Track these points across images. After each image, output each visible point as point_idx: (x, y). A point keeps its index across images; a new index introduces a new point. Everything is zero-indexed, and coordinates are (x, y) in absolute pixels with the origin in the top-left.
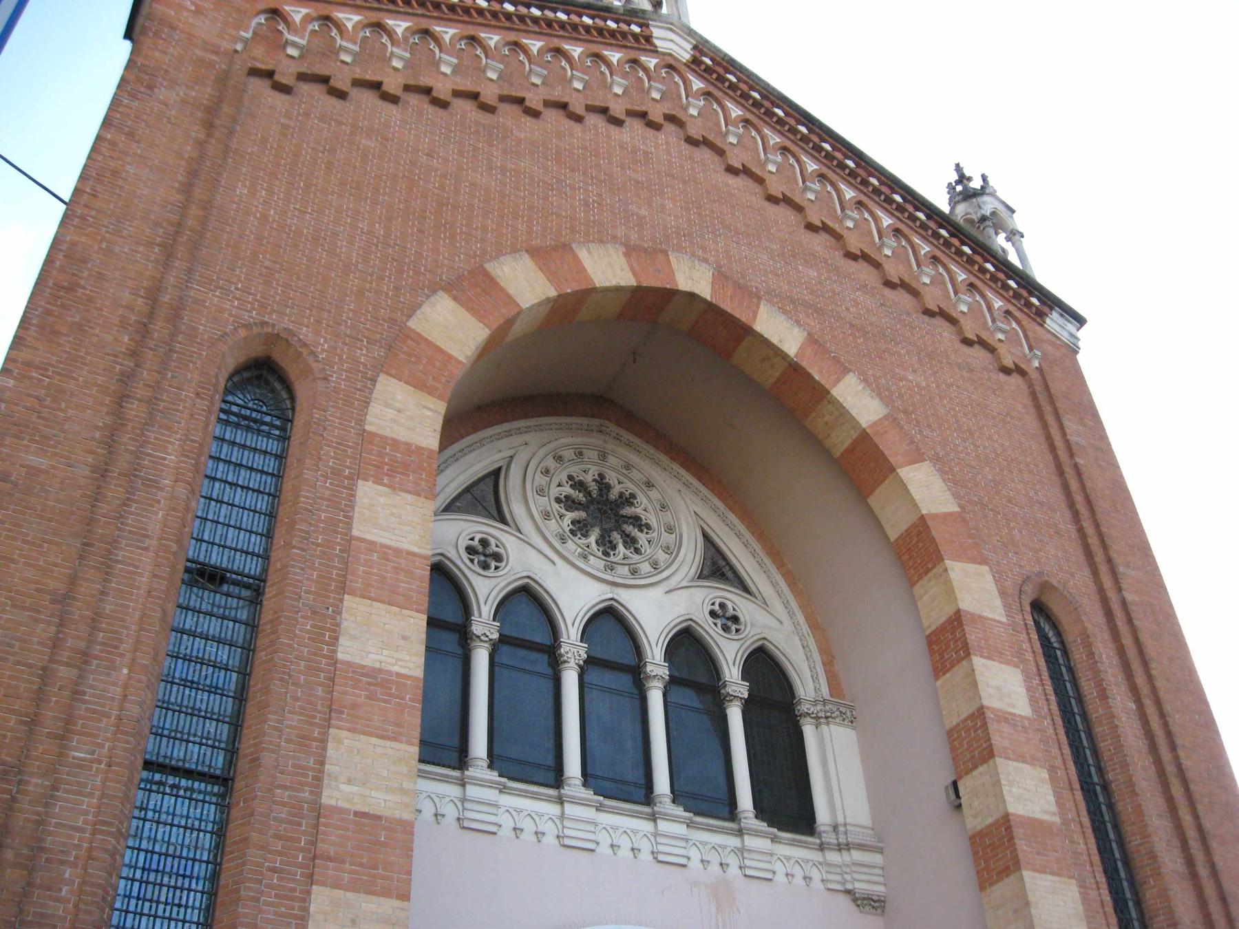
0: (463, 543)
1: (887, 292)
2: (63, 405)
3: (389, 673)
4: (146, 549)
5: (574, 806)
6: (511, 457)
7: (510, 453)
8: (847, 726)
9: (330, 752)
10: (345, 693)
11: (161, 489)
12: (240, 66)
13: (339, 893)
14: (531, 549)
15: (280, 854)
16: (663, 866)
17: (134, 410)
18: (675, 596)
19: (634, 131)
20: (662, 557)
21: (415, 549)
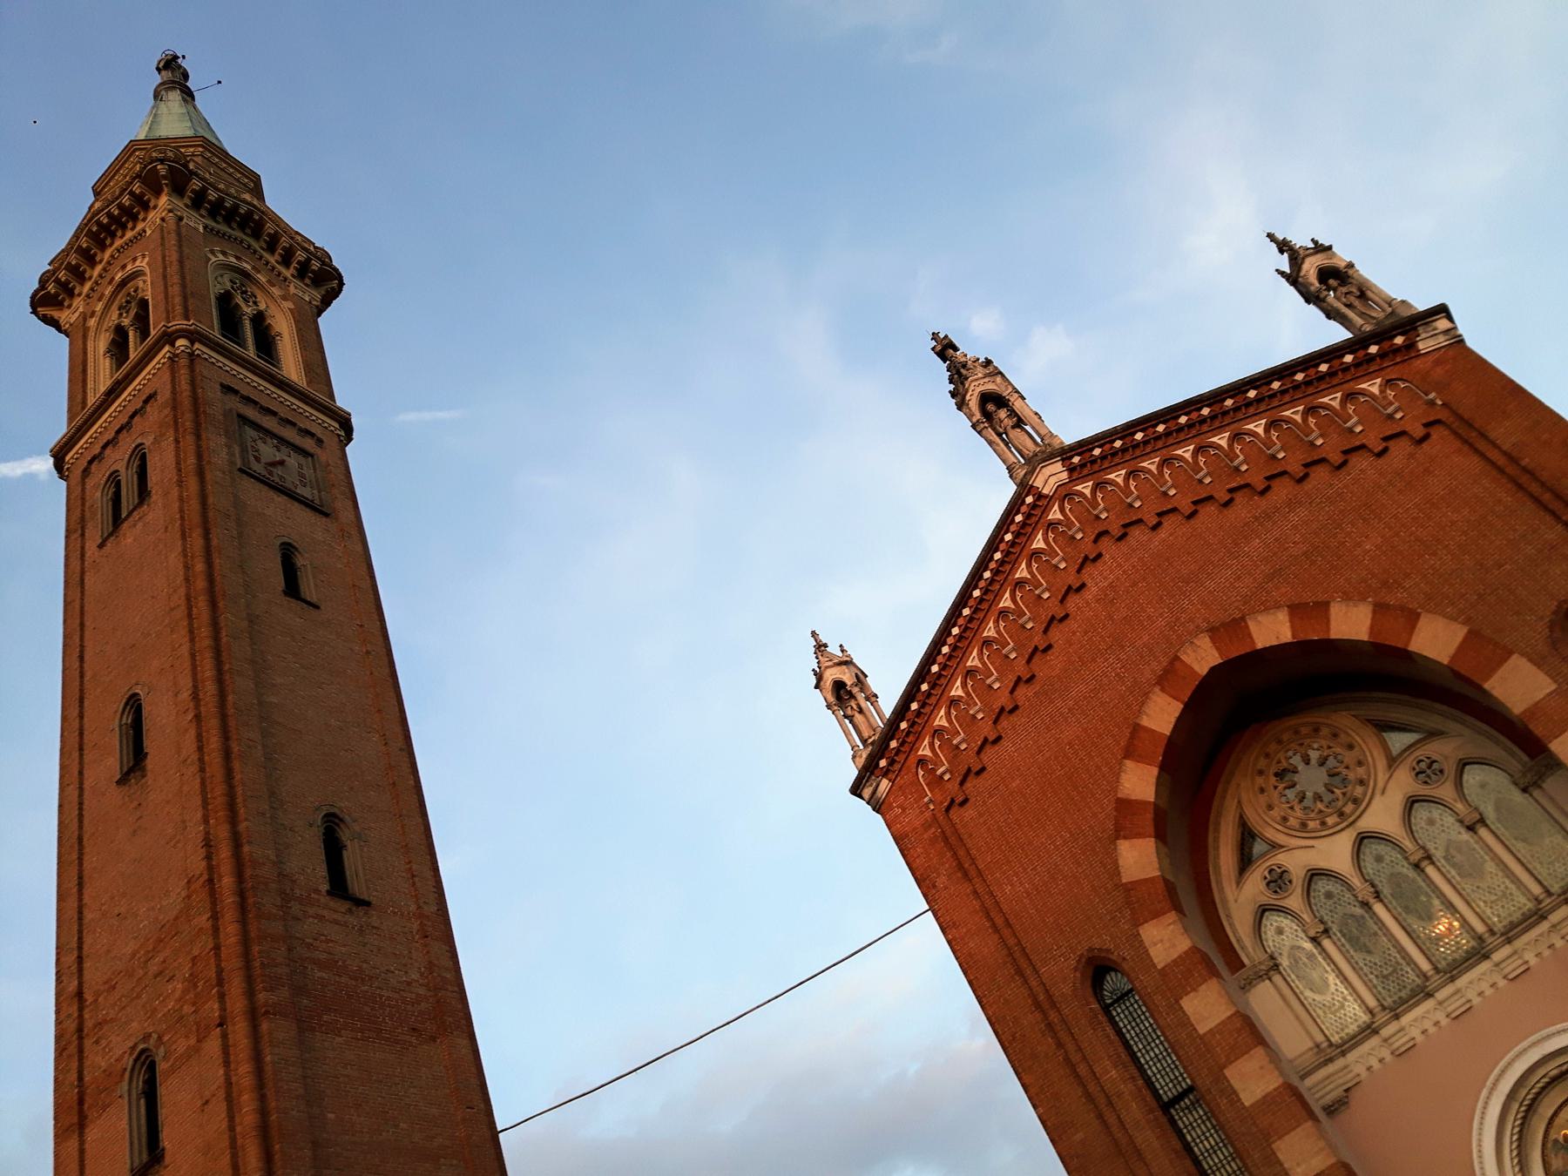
0: (1262, 886)
1: (1308, 485)
2: (1063, 1100)
5: (1440, 992)
6: (1239, 802)
11: (1123, 1093)
14: (1294, 851)
16: (1519, 979)
17: (1082, 1069)
18: (1389, 791)
19: (1096, 579)
20: (1361, 771)
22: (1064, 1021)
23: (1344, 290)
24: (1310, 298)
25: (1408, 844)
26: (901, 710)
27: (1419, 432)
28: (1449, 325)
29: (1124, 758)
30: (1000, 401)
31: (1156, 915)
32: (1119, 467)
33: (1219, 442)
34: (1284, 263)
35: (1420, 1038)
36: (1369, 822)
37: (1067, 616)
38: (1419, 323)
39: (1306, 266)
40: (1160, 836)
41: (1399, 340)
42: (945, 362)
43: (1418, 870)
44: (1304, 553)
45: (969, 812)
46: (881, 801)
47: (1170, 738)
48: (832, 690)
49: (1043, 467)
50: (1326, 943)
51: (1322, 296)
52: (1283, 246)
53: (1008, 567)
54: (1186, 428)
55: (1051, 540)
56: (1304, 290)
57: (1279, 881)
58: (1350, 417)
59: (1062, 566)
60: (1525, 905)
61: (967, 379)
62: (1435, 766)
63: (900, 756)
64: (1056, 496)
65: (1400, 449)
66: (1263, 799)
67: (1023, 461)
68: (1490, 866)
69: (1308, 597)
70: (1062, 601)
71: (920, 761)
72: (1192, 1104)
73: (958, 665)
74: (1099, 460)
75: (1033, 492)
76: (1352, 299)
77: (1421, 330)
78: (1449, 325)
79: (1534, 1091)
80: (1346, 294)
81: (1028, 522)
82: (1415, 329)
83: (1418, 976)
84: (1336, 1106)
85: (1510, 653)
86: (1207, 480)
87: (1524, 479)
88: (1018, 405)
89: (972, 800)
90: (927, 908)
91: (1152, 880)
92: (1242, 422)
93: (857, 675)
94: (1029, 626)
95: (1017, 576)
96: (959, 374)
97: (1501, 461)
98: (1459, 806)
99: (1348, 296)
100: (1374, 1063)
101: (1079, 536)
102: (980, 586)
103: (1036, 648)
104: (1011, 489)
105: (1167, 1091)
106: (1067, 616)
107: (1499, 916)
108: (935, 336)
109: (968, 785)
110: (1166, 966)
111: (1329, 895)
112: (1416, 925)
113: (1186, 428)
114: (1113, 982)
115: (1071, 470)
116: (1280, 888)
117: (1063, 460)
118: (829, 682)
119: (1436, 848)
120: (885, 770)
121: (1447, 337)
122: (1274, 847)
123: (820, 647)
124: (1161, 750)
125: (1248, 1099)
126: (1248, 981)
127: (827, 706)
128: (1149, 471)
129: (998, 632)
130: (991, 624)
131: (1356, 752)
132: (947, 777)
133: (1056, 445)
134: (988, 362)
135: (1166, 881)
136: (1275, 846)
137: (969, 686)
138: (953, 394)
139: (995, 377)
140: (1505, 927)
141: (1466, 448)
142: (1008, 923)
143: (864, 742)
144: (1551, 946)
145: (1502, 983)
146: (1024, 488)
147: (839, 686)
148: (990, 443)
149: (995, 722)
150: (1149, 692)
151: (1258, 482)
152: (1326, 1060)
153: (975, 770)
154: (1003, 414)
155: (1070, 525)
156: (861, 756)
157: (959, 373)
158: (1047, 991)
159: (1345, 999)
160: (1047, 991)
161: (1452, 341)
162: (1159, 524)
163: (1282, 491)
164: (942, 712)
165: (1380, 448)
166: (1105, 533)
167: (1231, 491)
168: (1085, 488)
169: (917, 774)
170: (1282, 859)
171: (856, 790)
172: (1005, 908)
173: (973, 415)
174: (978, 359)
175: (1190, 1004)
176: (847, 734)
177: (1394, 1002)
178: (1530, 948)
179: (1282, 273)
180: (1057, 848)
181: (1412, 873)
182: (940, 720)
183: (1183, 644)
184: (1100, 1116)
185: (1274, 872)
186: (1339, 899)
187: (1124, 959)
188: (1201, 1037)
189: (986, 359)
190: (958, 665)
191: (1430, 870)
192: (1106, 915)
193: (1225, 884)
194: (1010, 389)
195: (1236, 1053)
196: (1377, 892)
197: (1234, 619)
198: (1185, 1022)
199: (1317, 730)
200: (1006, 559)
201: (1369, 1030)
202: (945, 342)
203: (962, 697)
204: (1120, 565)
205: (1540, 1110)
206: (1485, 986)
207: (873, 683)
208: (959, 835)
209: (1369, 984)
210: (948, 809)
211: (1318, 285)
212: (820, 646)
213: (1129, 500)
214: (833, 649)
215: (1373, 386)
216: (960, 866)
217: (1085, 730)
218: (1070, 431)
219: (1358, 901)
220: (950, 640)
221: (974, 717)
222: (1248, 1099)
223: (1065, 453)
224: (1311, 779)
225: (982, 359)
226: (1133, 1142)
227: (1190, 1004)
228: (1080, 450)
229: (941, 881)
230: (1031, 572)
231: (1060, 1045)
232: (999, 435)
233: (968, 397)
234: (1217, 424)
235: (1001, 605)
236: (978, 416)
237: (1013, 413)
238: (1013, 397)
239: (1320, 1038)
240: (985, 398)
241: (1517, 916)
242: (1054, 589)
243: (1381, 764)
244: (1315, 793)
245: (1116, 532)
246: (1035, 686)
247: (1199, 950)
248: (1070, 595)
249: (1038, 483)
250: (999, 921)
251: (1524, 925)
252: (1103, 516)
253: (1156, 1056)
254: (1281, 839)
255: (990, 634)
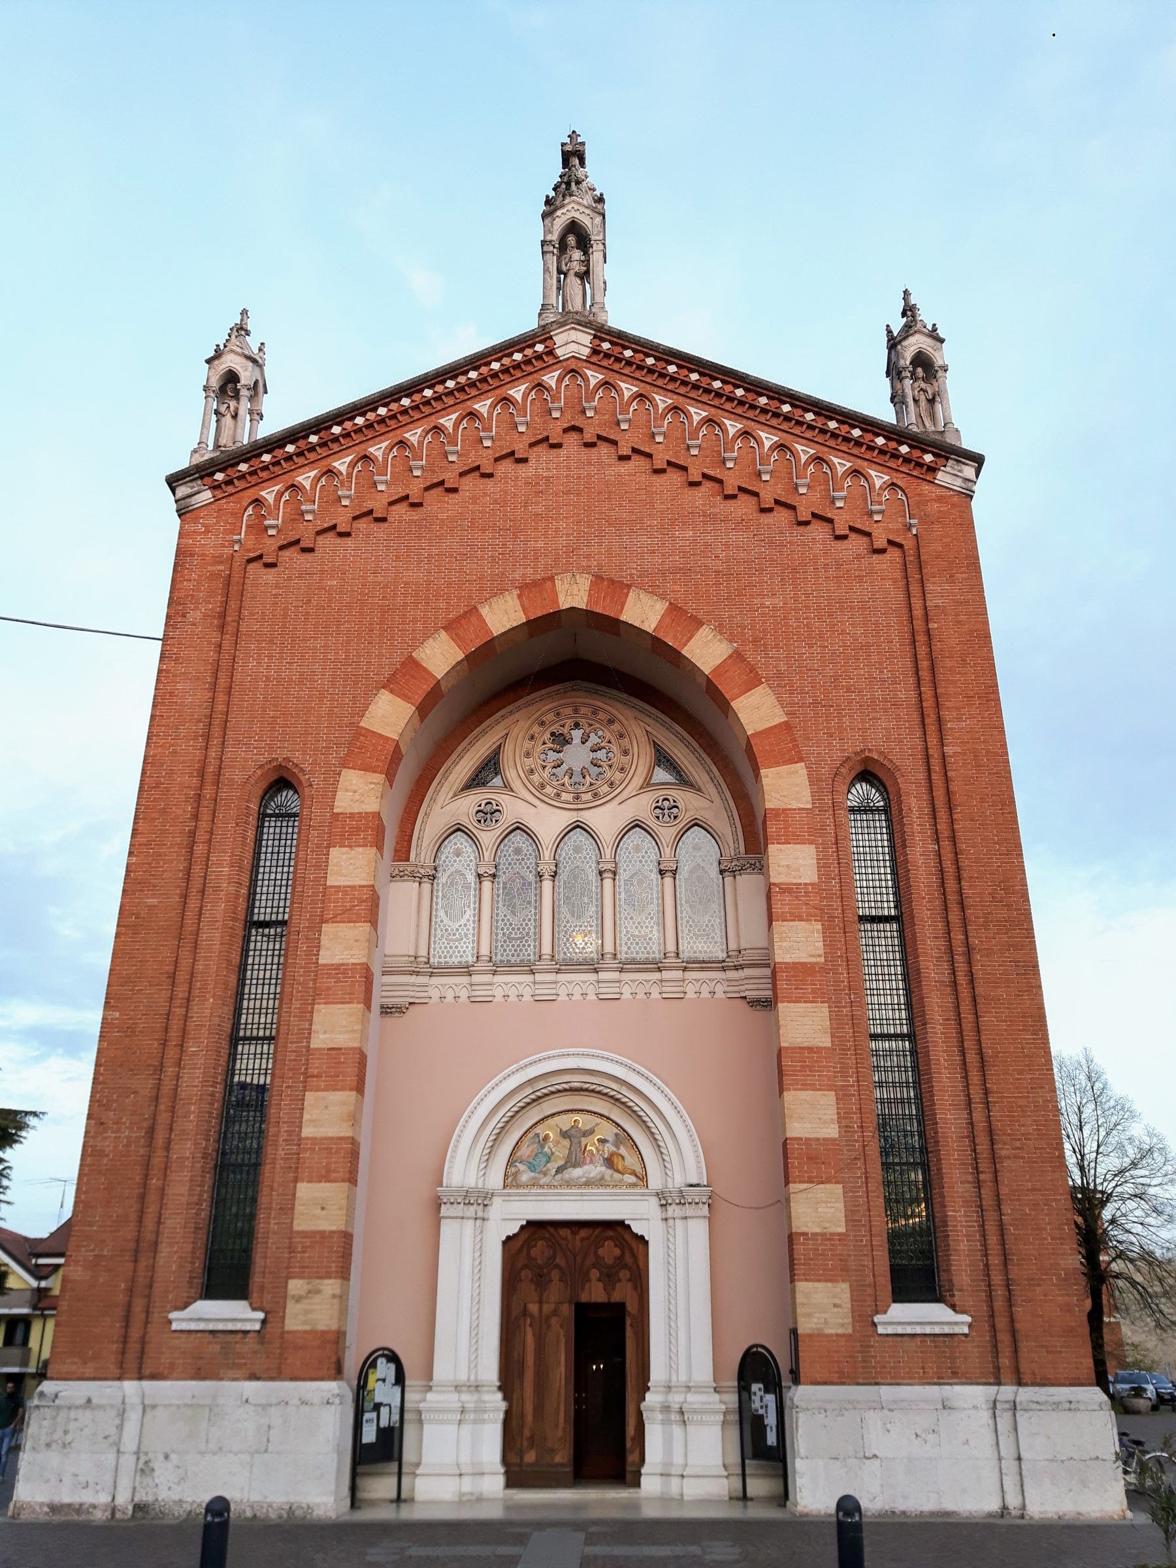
1: (766, 519)
3: (348, 964)
4: (217, 929)
7: (506, 732)
8: (756, 873)
9: (315, 1019)
10: (324, 983)
12: (238, 562)
13: (319, 1093)
15: (291, 1078)
17: (200, 849)
19: (542, 462)
20: (618, 776)
21: (365, 883)
22: (216, 801)
23: (923, 385)
24: (893, 371)
25: (608, 853)
26: (274, 443)
27: (880, 543)
28: (973, 477)
29: (443, 628)
30: (584, 243)
31: (366, 768)
32: (635, 382)
33: (729, 427)
34: (897, 325)
35: (499, 999)
36: (591, 818)
37: (490, 475)
38: (953, 456)
39: (912, 340)
40: (423, 710)
41: (928, 458)
42: (563, 168)
43: (599, 877)
44: (717, 572)
45: (270, 576)
46: (191, 508)
47: (494, 638)
48: (221, 376)
49: (573, 328)
50: (487, 885)
51: (903, 374)
52: (909, 311)
53: (474, 392)
54: (713, 394)
55: (530, 398)
56: (894, 359)
57: (489, 816)
58: (842, 489)
59: (522, 429)
60: (654, 953)
61: (571, 195)
62: (675, 810)
63: (241, 482)
64: (564, 364)
65: (856, 544)
66: (528, 744)
67: (560, 311)
68: (653, 908)
69: (691, 607)
70: (497, 460)
71: (257, 500)
72: (276, 935)
73: (360, 443)
74: (624, 362)
75: (548, 343)
76: (922, 398)
77: (950, 462)
78: (973, 477)
79: (550, 1088)
80: (922, 389)
81: (523, 366)
82: (947, 459)
83: (535, 954)
84: (393, 1010)
85: (801, 760)
86: (694, 452)
87: (921, 638)
88: (596, 257)
89: (280, 569)
90: (161, 637)
91: (387, 739)
92: (759, 426)
93: (256, 382)
94: (452, 458)
95: (476, 406)
96: (568, 185)
97: (918, 612)
98: (667, 852)
99: (922, 393)
100: (450, 995)
101: (556, 414)
102: (436, 389)
103: (442, 483)
104: (530, 324)
105: (261, 915)
106: (490, 475)
107: (629, 948)
108: (573, 135)
109: (286, 553)
110: (341, 814)
111: (518, 851)
112: (564, 910)
113: (713, 394)
114: (286, 798)
115: (595, 352)
116: (485, 821)
117: (595, 337)
118: (224, 366)
119: (625, 870)
120: (216, 483)
121: (963, 485)
122: (506, 787)
123: (241, 330)
124: (478, 643)
125: (325, 958)
126: (402, 874)
127: (204, 386)
128: (656, 406)
129: (421, 443)
130: (419, 431)
131: (625, 760)
132: (271, 532)
133: (601, 318)
134: (600, 200)
135: (397, 746)
136: (507, 786)
137: (356, 470)
138: (548, 202)
139: (596, 215)
140: (627, 959)
141: (902, 584)
142: (230, 692)
143: (217, 446)
144: (648, 994)
145: (592, 997)
146: (543, 334)
147: (231, 378)
148: (546, 270)
149: (355, 518)
150: (507, 590)
151: (731, 484)
152: (414, 972)
153: (303, 544)
154: (577, 255)
155: (555, 398)
156: (203, 456)
157: (568, 184)
158: (220, 768)
159: (466, 935)
160: (220, 768)
161: (965, 491)
162: (628, 458)
163: (743, 507)
164: (312, 474)
165: (842, 533)
166: (579, 430)
167: (705, 476)
168: (594, 377)
169: (245, 510)
170: (505, 800)
171: (173, 481)
172: (237, 677)
173: (551, 232)
174: (594, 190)
175: (338, 855)
176: (205, 425)
177: (501, 961)
178: (631, 985)
179: (889, 332)
180: (325, 660)
181: (593, 876)
182: (305, 479)
183: (567, 571)
184: (185, 897)
185: (490, 806)
186: (523, 859)
187: (311, 785)
188: (326, 887)
189: (602, 195)
190: (360, 443)
191: (608, 883)
192: (323, 741)
193: (445, 789)
194: (601, 237)
195: (347, 916)
196: (556, 872)
197: (621, 582)
198: (322, 866)
199: (611, 722)
200: (478, 383)
201: (467, 970)
202: (579, 148)
203: (342, 474)
204: (569, 468)
205: (544, 1105)
206: (577, 991)
207: (267, 403)
208: (243, 589)
209: (494, 935)
210: (250, 561)
211: (908, 363)
212: (242, 328)
213: (620, 417)
214: (253, 342)
215: (879, 479)
216: (223, 615)
217: (429, 582)
218: (618, 318)
219: (536, 870)
220: (371, 416)
221: (339, 498)
222: (325, 958)
223: (602, 332)
224: (577, 755)
225: (597, 193)
226: (197, 935)
227: (338, 855)
228: (615, 340)
229: (194, 615)
230: (490, 414)
231: (196, 817)
232: (559, 272)
233: (559, 213)
234: (739, 410)
235: (441, 421)
236: (555, 237)
237: (586, 262)
238: (597, 247)
239: (423, 952)
240: (574, 227)
241: (641, 956)
242: (498, 443)
243: (638, 781)
244: (570, 769)
245: (589, 436)
246: (415, 515)
247: (380, 819)
248: (507, 460)
249: (559, 339)
250: (223, 681)
251: (641, 966)
252: (589, 414)
253: (275, 880)
254: (516, 784)
255: (412, 439)
